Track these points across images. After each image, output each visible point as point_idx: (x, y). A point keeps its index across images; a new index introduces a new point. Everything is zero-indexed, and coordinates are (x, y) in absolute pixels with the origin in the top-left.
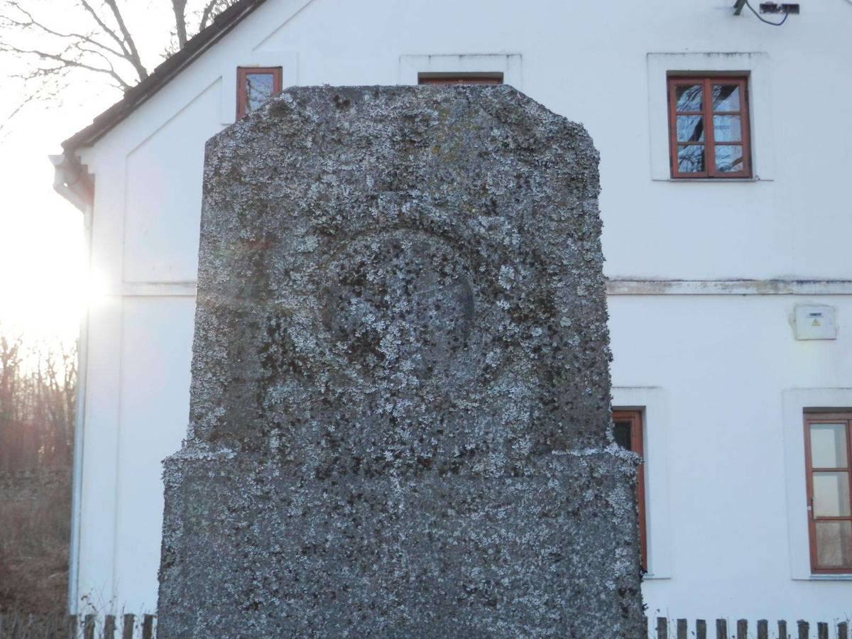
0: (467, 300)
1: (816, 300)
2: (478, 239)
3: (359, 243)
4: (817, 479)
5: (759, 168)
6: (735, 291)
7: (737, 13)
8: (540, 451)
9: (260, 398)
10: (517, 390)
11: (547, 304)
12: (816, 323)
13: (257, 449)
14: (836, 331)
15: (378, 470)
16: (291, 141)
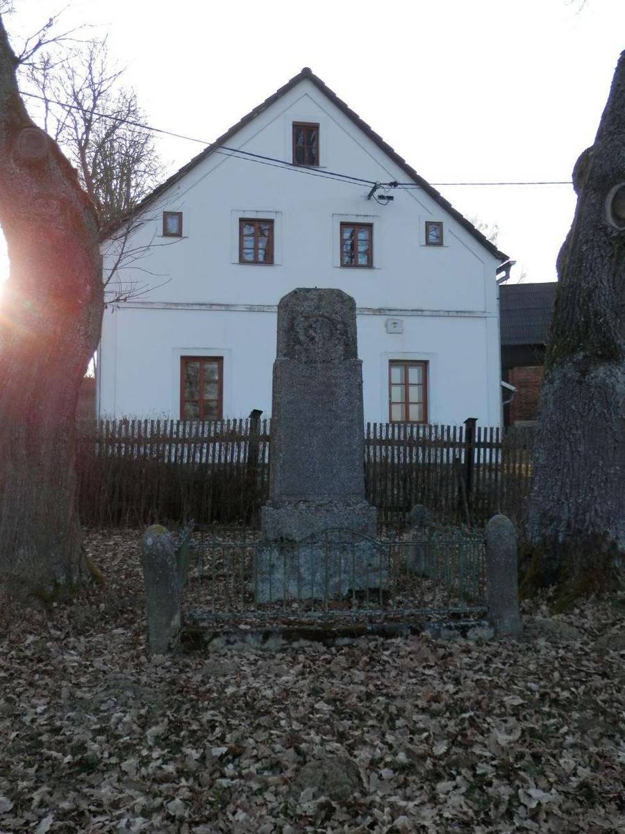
1: (395, 317)
2: (333, 319)
3: (311, 319)
4: (393, 406)
5: (376, 264)
8: (345, 359)
9: (293, 348)
10: (341, 348)
11: (346, 332)
12: (395, 327)
14: (403, 330)
15: (315, 362)
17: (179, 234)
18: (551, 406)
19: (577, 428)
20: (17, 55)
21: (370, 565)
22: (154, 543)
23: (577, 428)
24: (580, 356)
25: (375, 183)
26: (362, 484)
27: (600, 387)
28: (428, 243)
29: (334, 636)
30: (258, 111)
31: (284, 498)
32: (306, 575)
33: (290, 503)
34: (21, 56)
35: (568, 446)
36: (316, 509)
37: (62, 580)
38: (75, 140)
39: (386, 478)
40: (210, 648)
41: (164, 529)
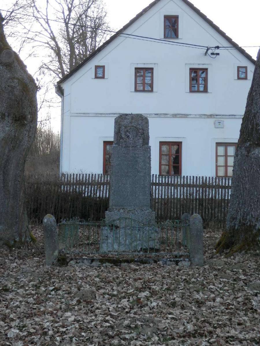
0: (137, 133)
1: (220, 119)
5: (209, 90)
6: (203, 117)
7: (206, 55)
8: (143, 146)
11: (144, 133)
12: (219, 124)
13: (119, 145)
14: (224, 126)
15: (129, 147)
16: (122, 119)
17: (103, 77)
18: (237, 167)
19: (246, 177)
20: (4, 17)
21: (151, 237)
22: (47, 221)
23: (246, 177)
24: (248, 144)
25: (207, 47)
26: (149, 202)
27: (256, 159)
28: (239, 78)
29: (121, 262)
30: (145, 11)
31: (114, 207)
32: (122, 241)
33: (116, 209)
34: (5, 17)
35: (241, 185)
36: (128, 212)
37: (17, 239)
38: (63, 19)
39: (221, 206)
40: (69, 264)
41: (52, 216)
